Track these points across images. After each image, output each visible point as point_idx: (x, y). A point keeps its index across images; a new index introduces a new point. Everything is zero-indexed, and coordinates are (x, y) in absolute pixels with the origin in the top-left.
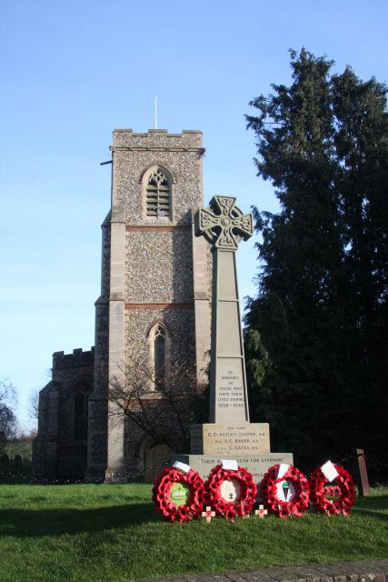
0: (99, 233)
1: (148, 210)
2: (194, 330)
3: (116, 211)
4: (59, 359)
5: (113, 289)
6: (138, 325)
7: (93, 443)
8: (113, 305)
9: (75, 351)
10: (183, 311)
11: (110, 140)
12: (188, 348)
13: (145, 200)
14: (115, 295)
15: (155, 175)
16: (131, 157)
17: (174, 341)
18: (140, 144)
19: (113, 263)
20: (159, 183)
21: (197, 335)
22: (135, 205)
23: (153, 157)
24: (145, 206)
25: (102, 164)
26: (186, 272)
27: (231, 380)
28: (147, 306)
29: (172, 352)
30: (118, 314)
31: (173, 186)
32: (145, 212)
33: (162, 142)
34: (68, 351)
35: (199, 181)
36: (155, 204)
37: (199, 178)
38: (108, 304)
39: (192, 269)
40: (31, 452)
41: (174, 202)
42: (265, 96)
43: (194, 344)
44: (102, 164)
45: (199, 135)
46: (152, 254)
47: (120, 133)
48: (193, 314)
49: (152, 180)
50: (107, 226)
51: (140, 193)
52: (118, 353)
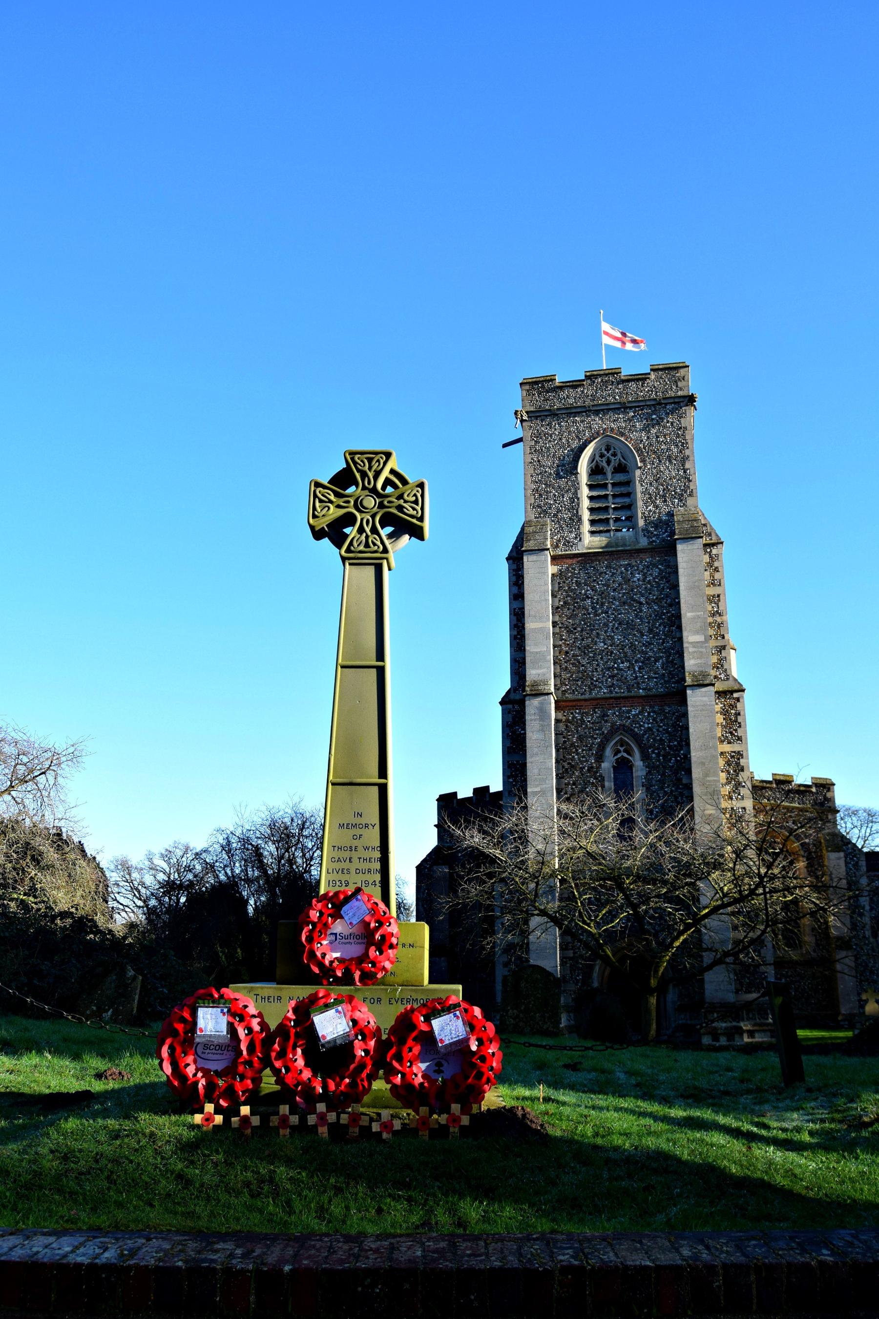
0: (503, 570)
1: (591, 498)
2: (688, 744)
3: (531, 529)
4: (437, 800)
5: (532, 674)
6: (580, 738)
7: (505, 959)
8: (532, 706)
9: (476, 791)
10: (667, 709)
11: (516, 400)
12: (680, 780)
13: (586, 503)
14: (535, 684)
15: (602, 456)
16: (556, 428)
17: (651, 768)
18: (571, 401)
19: (530, 625)
20: (609, 470)
21: (693, 754)
22: (566, 515)
23: (597, 423)
24: (586, 516)
25: (505, 446)
26: (669, 663)
27: (358, 832)
28: (597, 703)
29: (648, 787)
30: (541, 719)
31: (638, 472)
32: (586, 527)
33: (613, 394)
34: (465, 792)
35: (685, 459)
36: (606, 509)
37: (687, 452)
38: (522, 703)
39: (680, 628)
40: (147, 1081)
41: (640, 503)
42: (724, 618)
43: (689, 772)
44: (505, 446)
45: (682, 372)
46: (602, 604)
47: (534, 386)
48: (685, 715)
49: (597, 466)
50: (516, 558)
51: (576, 493)
52: (543, 792)
